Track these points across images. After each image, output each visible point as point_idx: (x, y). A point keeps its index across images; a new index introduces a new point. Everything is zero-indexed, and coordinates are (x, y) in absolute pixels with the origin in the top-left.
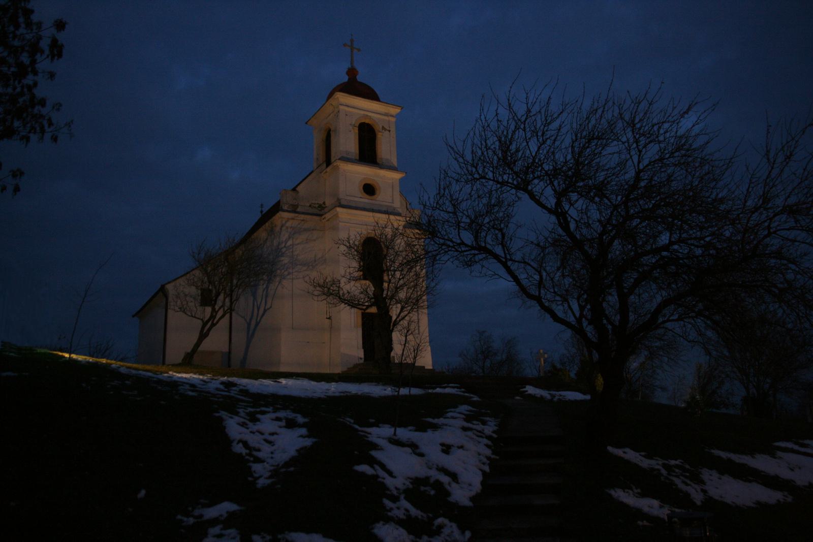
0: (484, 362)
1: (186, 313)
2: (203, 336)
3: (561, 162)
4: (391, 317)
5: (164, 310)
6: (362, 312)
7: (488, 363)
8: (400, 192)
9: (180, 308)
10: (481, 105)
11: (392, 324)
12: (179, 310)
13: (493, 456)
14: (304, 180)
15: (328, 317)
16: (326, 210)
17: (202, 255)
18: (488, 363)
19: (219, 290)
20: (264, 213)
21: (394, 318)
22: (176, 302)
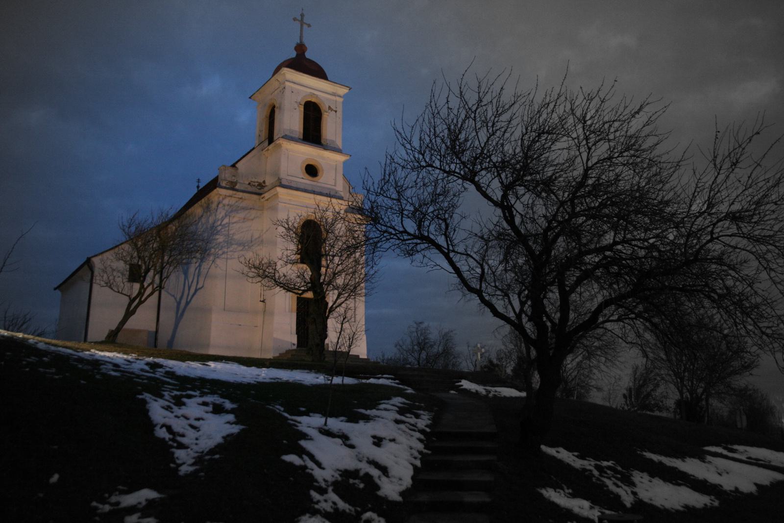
1: (112, 289)
4: (327, 304)
6: (297, 297)
9: (107, 283)
11: (328, 311)
16: (266, 189)
17: (133, 229)
19: (149, 266)
20: (200, 188)
21: (330, 305)
22: (102, 277)
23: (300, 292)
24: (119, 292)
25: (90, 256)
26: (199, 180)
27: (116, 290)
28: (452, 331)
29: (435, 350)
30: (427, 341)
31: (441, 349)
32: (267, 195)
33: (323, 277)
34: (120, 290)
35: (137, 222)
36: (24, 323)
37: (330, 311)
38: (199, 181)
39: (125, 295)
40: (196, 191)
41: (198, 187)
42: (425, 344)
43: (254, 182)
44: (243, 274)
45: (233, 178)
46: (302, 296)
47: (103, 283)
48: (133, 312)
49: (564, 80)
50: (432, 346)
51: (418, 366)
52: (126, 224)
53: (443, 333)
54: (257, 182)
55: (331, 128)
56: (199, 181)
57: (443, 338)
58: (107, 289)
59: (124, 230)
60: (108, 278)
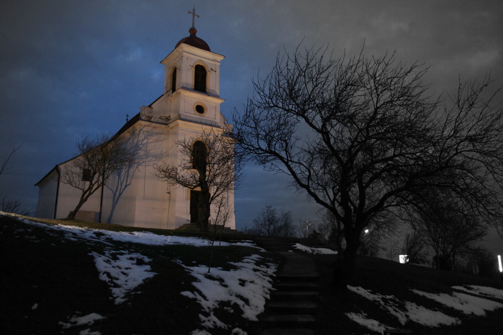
1: (72, 185)
4: (210, 194)
6: (191, 190)
9: (68, 181)
11: (210, 199)
16: (170, 121)
17: (85, 147)
19: (95, 170)
20: (128, 121)
21: (212, 195)
22: (66, 177)
23: (193, 187)
24: (76, 187)
25: (57, 164)
29: (279, 224)
30: (274, 218)
32: (171, 125)
33: (207, 178)
34: (77, 186)
36: (15, 207)
37: (212, 200)
38: (127, 116)
39: (80, 189)
40: (125, 122)
42: (273, 220)
43: (163, 117)
44: (156, 175)
45: (150, 114)
48: (86, 200)
49: (362, 51)
50: (277, 222)
53: (284, 214)
54: (165, 117)
55: (212, 82)
56: (127, 116)
59: (79, 147)
60: (70, 178)
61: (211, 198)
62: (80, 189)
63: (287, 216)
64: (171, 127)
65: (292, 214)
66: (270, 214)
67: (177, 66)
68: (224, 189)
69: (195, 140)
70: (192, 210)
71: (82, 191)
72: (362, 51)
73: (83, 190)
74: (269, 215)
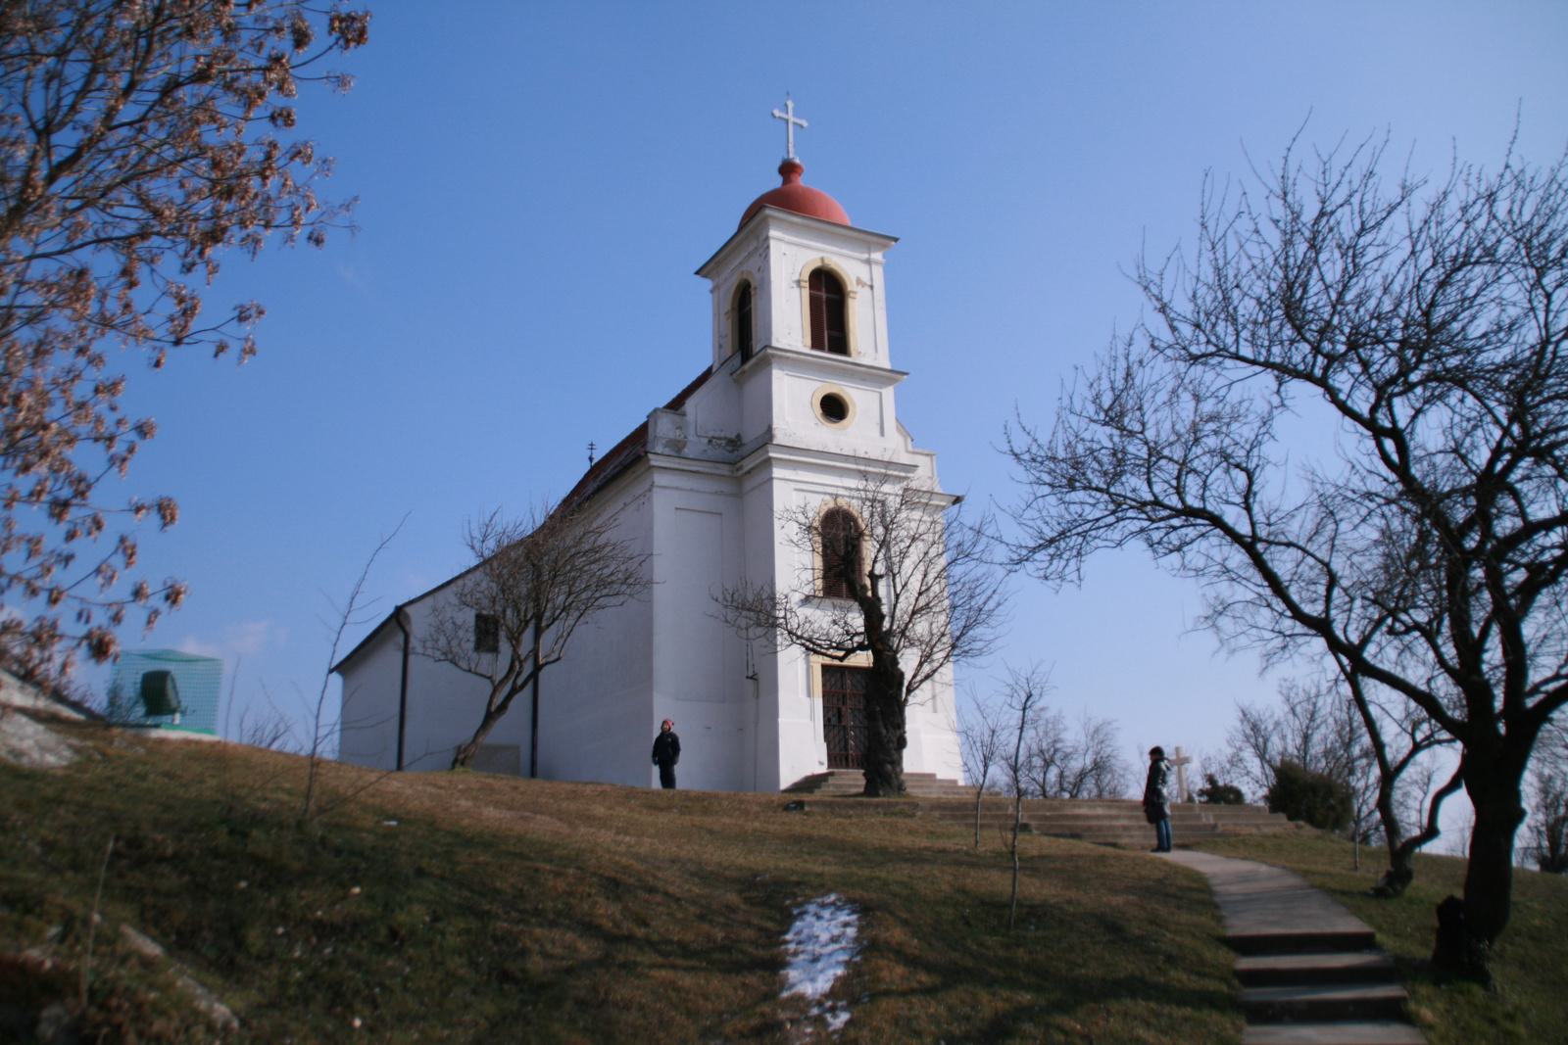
0: (1045, 774)
1: (456, 664)
2: (490, 717)
3: (1365, 344)
4: (902, 675)
5: (399, 656)
6: (825, 668)
7: (1053, 774)
8: (897, 420)
9: (445, 654)
10: (1204, 226)
11: (904, 689)
12: (442, 658)
13: (783, 947)
14: (78, 583)
15: (750, 674)
16: (745, 450)
17: (491, 544)
18: (1053, 774)
19: (525, 616)
20: (595, 461)
21: (908, 677)
22: (437, 641)
23: (841, 654)
24: (470, 671)
25: (400, 603)
26: (122, 540)
27: (465, 666)
28: (1109, 723)
29: (1076, 765)
30: (1059, 745)
31: (1088, 761)
32: (748, 464)
33: (887, 620)
34: (473, 667)
35: (499, 529)
36: (275, 739)
37: (909, 691)
38: (592, 447)
39: (482, 675)
40: (586, 467)
41: (591, 459)
42: (1056, 751)
43: (720, 439)
44: (727, 621)
45: (678, 432)
46: (846, 663)
47: (438, 654)
48: (503, 707)
49: (1512, 143)
50: (1066, 756)
51: (1041, 797)
52: (477, 534)
53: (1092, 730)
54: (725, 438)
55: (865, 318)
56: (592, 447)
57: (1092, 739)
58: (447, 665)
59: (473, 547)
60: (449, 643)
61: (906, 683)
62: (482, 675)
63: (1098, 734)
64: (746, 469)
65: (1118, 729)
66: (1046, 733)
67: (751, 281)
68: (947, 656)
69: (825, 509)
70: (831, 735)
71: (488, 682)
72: (1512, 143)
73: (490, 678)
74: (1041, 734)
